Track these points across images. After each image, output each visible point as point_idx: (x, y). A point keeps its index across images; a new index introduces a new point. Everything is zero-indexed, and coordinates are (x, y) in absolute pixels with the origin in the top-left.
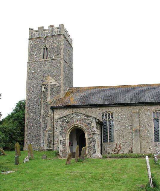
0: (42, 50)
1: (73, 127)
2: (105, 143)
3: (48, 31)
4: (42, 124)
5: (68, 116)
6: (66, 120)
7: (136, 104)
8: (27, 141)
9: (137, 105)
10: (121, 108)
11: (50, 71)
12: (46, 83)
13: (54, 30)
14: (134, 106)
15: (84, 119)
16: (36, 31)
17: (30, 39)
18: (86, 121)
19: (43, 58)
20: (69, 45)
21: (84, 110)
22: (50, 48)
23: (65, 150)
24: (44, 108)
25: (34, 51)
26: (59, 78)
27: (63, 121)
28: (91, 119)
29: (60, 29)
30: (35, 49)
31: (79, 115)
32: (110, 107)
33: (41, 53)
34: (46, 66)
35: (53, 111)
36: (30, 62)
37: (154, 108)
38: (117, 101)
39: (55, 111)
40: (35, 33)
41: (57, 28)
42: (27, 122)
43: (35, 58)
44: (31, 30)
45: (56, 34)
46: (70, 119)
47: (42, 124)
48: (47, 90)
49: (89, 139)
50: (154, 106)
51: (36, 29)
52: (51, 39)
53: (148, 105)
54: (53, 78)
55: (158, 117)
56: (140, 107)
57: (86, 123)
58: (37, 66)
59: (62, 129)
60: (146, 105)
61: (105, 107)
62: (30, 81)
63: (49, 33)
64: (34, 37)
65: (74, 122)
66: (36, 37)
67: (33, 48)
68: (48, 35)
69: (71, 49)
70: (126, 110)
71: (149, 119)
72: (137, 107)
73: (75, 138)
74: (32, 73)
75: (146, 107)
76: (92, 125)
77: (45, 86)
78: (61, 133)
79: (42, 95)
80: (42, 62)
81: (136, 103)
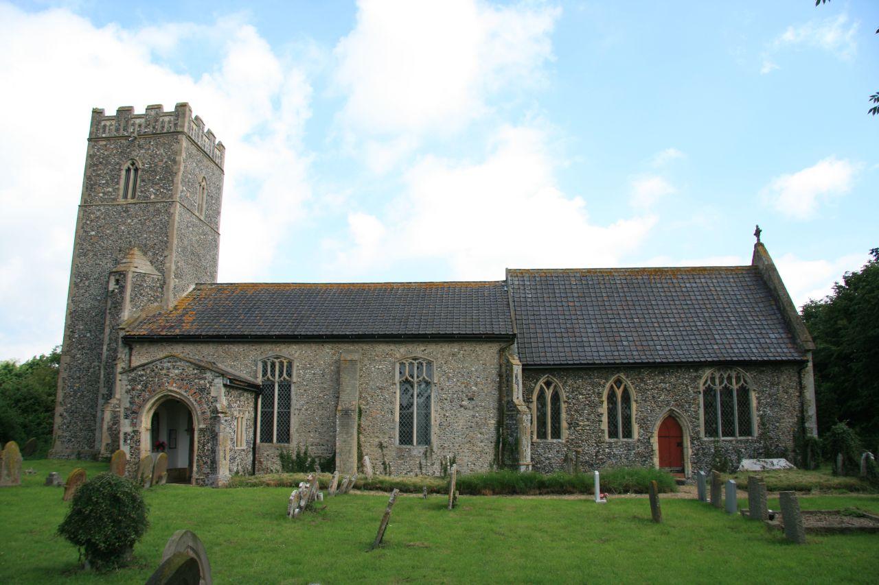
0: (123, 173)
1: (162, 397)
2: (266, 444)
3: (143, 120)
4: (102, 384)
5: (151, 366)
6: (142, 375)
7: (352, 338)
8: (60, 433)
9: (358, 342)
10: (314, 347)
11: (139, 235)
12: (121, 268)
13: (161, 120)
14: (348, 342)
15: (192, 376)
16: (110, 118)
17: (93, 139)
18: (196, 381)
19: (125, 196)
20: (206, 162)
21: (213, 351)
22: (143, 169)
23: (137, 460)
24: (110, 339)
25: (99, 175)
26: (162, 256)
27: (134, 380)
28: (209, 375)
29: (177, 116)
30: (103, 170)
31: (179, 363)
32: (284, 343)
33: (118, 183)
34: (129, 221)
35: (131, 349)
36: (85, 207)
37: (402, 350)
38: (301, 331)
39: (137, 348)
40: (108, 123)
41: (169, 114)
42: (65, 376)
43: (101, 195)
44: (97, 114)
45: (165, 131)
46: (153, 374)
47: (102, 384)
48: (122, 289)
49: (698, 426)
50: (404, 346)
51: (111, 111)
52: (150, 142)
53: (387, 342)
54: (145, 254)
55: (413, 378)
56: (365, 347)
57: (195, 387)
58: (104, 219)
59: (131, 403)
60: (380, 342)
61: (272, 343)
62: (83, 259)
63: (146, 127)
64: (104, 135)
65: (163, 384)
66: (108, 135)
67: (97, 165)
68: (143, 130)
69: (217, 172)
70: (326, 354)
71: (387, 381)
72: (357, 347)
73: (186, 428)
74: (88, 238)
75: (381, 349)
76: (212, 394)
77: (117, 277)
78: (129, 412)
79: (109, 303)
80: (119, 208)
81: (352, 335)
